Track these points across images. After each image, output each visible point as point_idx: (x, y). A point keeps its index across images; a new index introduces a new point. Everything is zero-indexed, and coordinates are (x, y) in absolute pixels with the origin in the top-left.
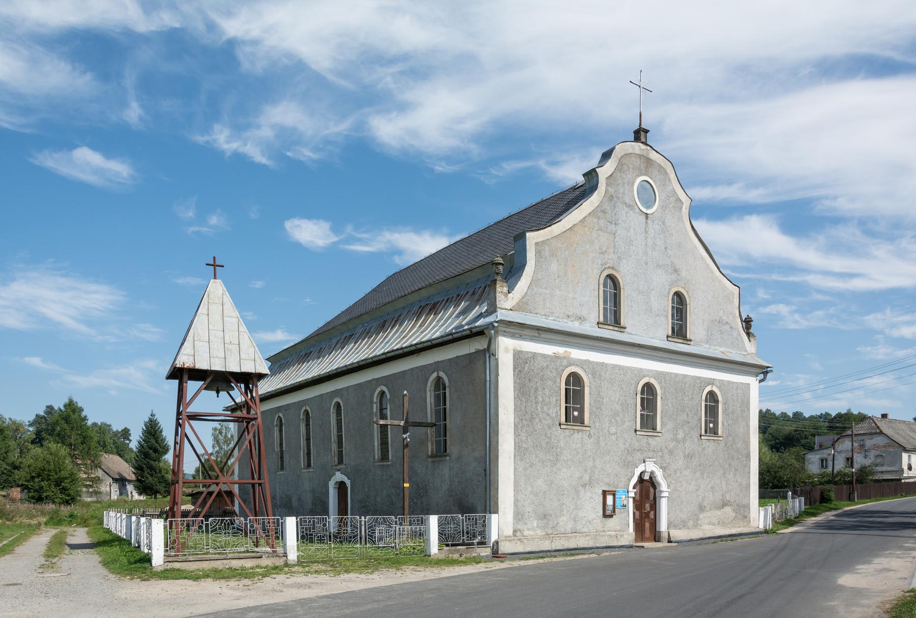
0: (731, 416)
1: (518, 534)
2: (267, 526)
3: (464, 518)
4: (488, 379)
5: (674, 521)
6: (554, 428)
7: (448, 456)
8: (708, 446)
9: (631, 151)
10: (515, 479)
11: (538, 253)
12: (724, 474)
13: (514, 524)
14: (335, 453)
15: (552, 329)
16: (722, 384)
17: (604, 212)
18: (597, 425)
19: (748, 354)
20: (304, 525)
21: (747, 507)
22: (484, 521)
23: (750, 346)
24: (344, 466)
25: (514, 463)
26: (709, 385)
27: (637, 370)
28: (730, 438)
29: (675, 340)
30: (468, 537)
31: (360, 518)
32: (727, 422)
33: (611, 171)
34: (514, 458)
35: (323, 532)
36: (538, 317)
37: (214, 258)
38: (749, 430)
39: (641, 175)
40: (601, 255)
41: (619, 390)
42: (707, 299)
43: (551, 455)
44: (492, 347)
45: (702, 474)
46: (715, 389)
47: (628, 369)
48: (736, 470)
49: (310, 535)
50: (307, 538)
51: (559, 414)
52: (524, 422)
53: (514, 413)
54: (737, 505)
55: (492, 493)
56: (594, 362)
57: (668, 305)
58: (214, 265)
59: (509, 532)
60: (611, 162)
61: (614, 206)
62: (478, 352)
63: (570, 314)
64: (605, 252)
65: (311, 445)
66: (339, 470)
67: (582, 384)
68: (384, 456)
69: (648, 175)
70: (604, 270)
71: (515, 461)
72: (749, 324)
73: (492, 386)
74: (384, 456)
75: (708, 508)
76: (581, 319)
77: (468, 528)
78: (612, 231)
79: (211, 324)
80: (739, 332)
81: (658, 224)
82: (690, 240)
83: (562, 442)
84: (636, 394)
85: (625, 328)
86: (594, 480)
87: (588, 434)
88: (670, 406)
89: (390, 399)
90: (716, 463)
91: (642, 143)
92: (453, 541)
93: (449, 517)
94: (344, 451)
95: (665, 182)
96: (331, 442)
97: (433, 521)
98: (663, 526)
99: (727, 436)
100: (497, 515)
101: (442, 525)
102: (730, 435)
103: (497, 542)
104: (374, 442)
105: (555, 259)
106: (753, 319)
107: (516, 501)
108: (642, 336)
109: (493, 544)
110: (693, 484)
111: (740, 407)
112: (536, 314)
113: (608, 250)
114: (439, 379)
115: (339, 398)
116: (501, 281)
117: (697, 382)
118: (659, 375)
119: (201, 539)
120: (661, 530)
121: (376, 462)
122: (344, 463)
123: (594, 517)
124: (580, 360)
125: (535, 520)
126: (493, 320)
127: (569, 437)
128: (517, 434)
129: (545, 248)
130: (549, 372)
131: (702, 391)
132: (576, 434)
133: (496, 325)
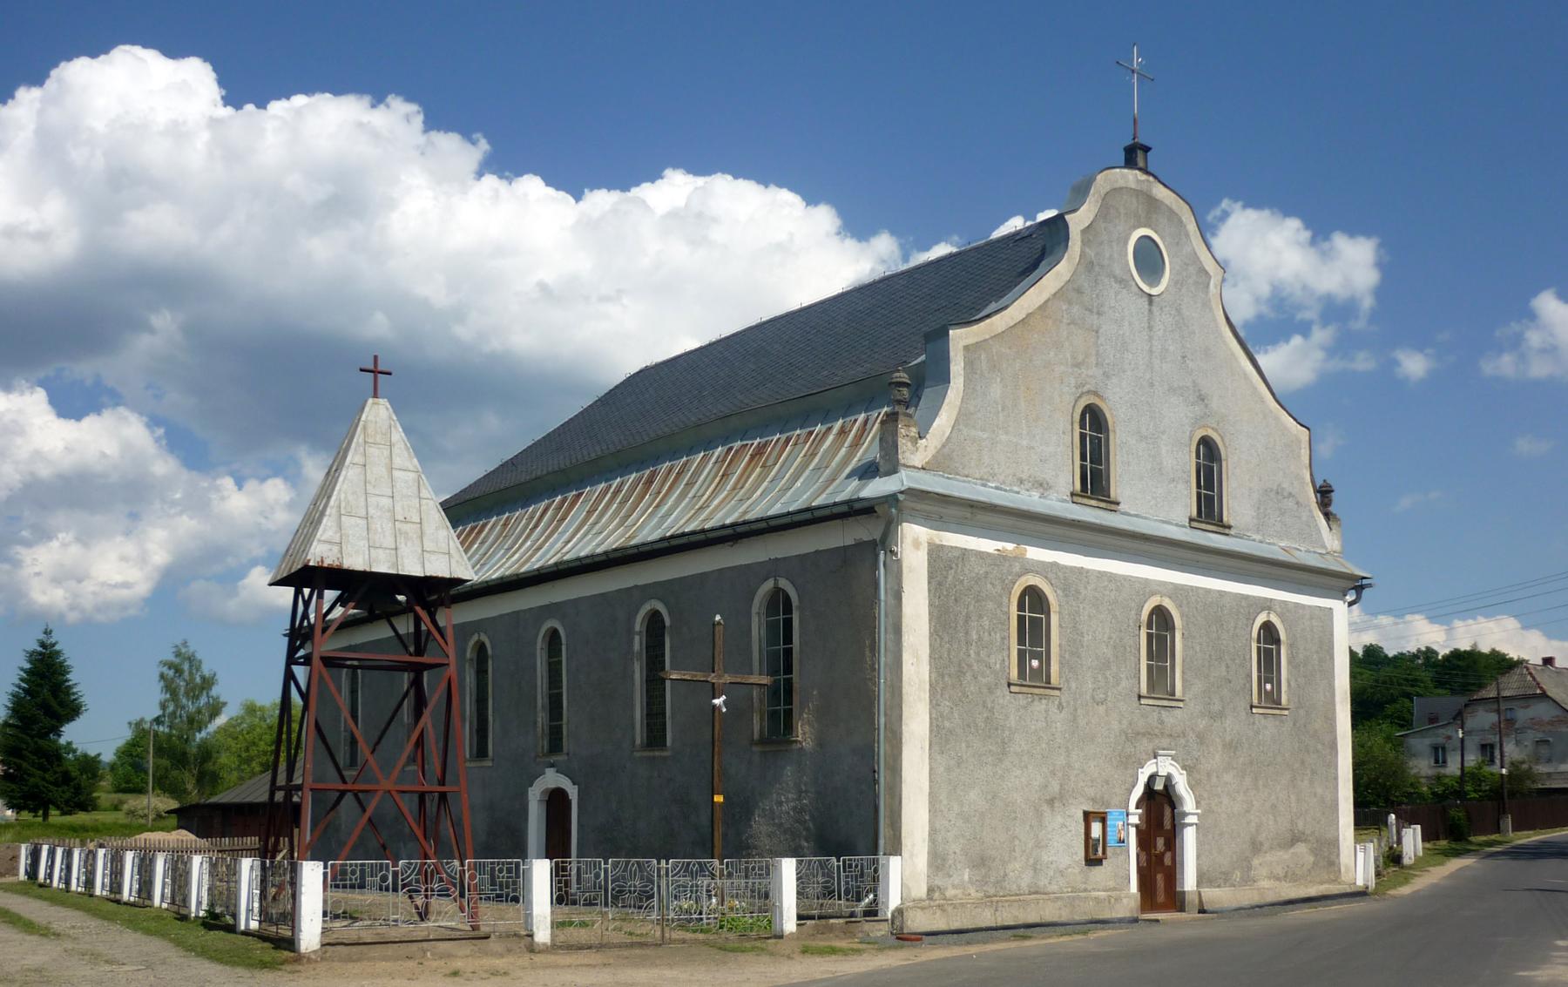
2: (499, 878)
3: (841, 863)
6: (999, 692)
9: (1121, 183)
11: (970, 365)
13: (928, 876)
14: (543, 729)
16: (1285, 609)
18: (1073, 685)
21: (1334, 843)
25: (930, 759)
26: (1262, 610)
28: (1302, 712)
29: (1203, 526)
31: (659, 863)
32: (1296, 681)
34: (930, 749)
36: (969, 482)
40: (1076, 369)
45: (1256, 779)
46: (1274, 619)
47: (1125, 580)
48: (1314, 772)
51: (1007, 664)
52: (946, 679)
53: (930, 662)
56: (1066, 567)
57: (1188, 461)
58: (375, 372)
59: (920, 891)
62: (860, 545)
63: (1024, 476)
66: (552, 766)
70: (1080, 397)
74: (655, 735)
75: (1266, 846)
76: (1043, 486)
77: (847, 883)
78: (1092, 325)
80: (1311, 511)
83: (1012, 717)
84: (1140, 627)
85: (1118, 504)
87: (1057, 703)
88: (1198, 648)
89: (671, 626)
91: (1140, 169)
96: (536, 707)
98: (1189, 881)
103: (899, 912)
107: (933, 832)
108: (1146, 518)
112: (967, 476)
113: (1087, 360)
117: (1243, 604)
118: (1177, 591)
122: (565, 749)
125: (965, 868)
128: (934, 702)
129: (980, 355)
130: (989, 586)
132: (1036, 703)
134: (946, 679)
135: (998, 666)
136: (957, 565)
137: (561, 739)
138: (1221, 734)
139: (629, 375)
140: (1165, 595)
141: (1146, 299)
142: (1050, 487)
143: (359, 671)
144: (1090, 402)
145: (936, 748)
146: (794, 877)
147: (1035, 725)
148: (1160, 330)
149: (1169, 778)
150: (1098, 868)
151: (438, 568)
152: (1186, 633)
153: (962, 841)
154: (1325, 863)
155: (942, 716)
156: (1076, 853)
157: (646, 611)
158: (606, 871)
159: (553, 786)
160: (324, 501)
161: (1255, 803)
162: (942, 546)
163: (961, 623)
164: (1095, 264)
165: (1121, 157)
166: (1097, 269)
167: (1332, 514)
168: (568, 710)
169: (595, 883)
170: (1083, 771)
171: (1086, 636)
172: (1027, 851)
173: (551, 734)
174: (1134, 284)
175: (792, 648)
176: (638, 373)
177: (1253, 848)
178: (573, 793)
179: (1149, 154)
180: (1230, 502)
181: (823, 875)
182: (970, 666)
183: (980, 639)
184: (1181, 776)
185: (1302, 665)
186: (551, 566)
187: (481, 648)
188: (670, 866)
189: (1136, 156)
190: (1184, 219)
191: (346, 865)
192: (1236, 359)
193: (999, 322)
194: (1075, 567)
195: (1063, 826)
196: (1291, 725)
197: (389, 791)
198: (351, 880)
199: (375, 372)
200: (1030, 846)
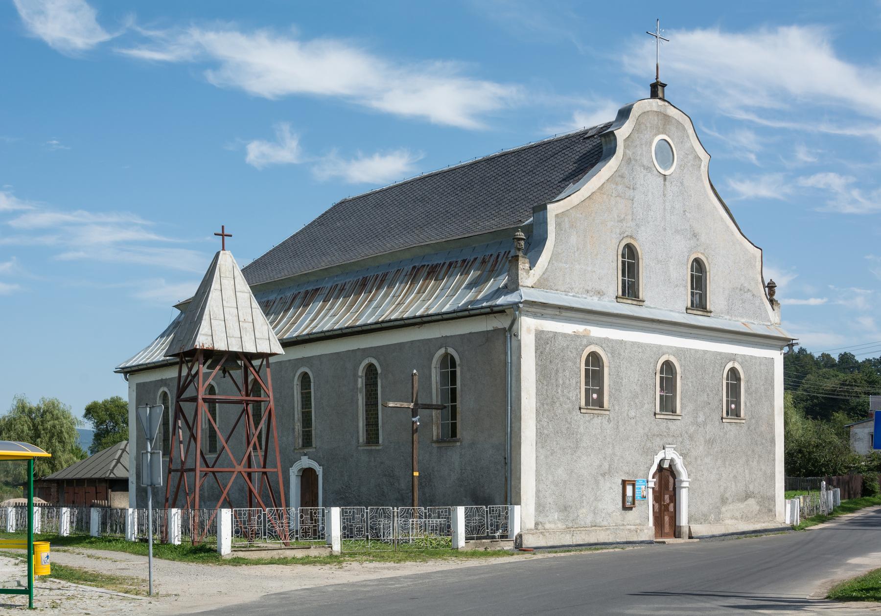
4: (509, 361)
5: (695, 514)
7: (458, 441)
9: (648, 109)
11: (558, 225)
12: (747, 461)
13: (535, 517)
14: (299, 434)
16: (744, 360)
17: (622, 177)
18: (617, 408)
21: (772, 499)
22: (507, 513)
25: (536, 451)
28: (753, 421)
29: (695, 312)
30: (492, 530)
32: (750, 402)
33: (629, 132)
40: (619, 224)
41: (638, 370)
45: (724, 461)
46: (737, 366)
48: (760, 456)
50: (242, 532)
51: (579, 397)
52: (545, 406)
53: (536, 397)
54: (762, 497)
56: (613, 340)
58: (223, 235)
59: (531, 525)
60: (629, 122)
62: (496, 330)
63: (589, 288)
66: (305, 455)
69: (665, 134)
71: (536, 449)
74: (372, 436)
75: (730, 500)
77: (491, 520)
80: (761, 300)
82: (709, 200)
89: (381, 373)
90: (739, 449)
91: (660, 99)
92: (478, 534)
97: (335, 513)
98: (684, 520)
104: (358, 422)
107: (538, 491)
110: (714, 472)
111: (764, 385)
112: (557, 290)
113: (626, 217)
116: (523, 257)
118: (680, 352)
120: (681, 525)
121: (360, 446)
122: (314, 446)
126: (517, 300)
127: (589, 421)
130: (569, 353)
131: (723, 368)
132: (595, 419)
134: (545, 406)
135: (574, 398)
136: (551, 341)
140: (671, 354)
141: (662, 179)
142: (604, 294)
143: (217, 404)
145: (540, 445)
149: (672, 460)
150: (630, 511)
152: (683, 376)
158: (367, 512)
164: (632, 159)
166: (633, 162)
167: (775, 301)
169: (361, 519)
170: (622, 457)
171: (624, 379)
175: (456, 388)
177: (722, 501)
178: (319, 470)
182: (558, 398)
183: (564, 383)
184: (679, 460)
185: (754, 393)
189: (658, 91)
190: (686, 126)
191: (241, 510)
193: (576, 199)
195: (611, 488)
197: (240, 472)
198: (244, 518)
199: (223, 235)
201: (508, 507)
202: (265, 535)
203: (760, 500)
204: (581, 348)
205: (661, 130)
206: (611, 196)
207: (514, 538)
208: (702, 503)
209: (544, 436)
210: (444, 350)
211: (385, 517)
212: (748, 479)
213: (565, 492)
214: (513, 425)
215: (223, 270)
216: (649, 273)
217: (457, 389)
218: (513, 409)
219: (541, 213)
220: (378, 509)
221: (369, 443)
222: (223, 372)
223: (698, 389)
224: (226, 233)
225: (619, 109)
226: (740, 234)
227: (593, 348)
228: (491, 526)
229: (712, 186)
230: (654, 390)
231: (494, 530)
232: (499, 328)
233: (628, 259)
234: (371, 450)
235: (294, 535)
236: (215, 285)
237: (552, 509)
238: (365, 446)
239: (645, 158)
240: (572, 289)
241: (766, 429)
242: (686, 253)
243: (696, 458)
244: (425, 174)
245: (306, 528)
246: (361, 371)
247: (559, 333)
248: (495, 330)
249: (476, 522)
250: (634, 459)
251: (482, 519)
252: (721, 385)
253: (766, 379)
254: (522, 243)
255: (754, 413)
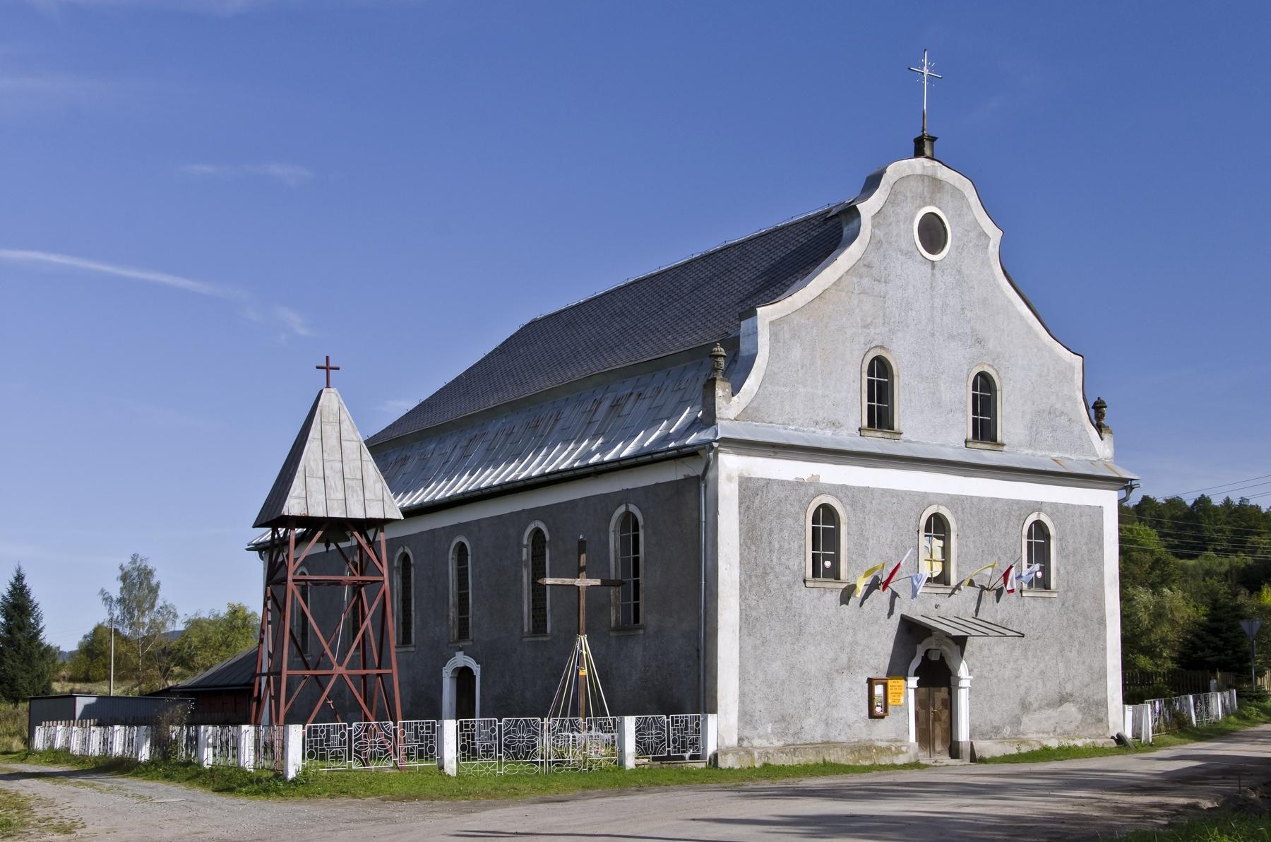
0: (1072, 558)
1: (745, 744)
2: (420, 733)
3: (670, 720)
4: (703, 520)
5: (980, 725)
6: (796, 588)
7: (641, 628)
8: (1034, 608)
9: (909, 172)
10: (740, 663)
11: (774, 336)
12: (1062, 650)
13: (739, 729)
14: (454, 621)
15: (793, 445)
16: (1055, 509)
17: (868, 267)
19: (1099, 460)
20: (465, 731)
21: (1103, 704)
22: (698, 725)
23: (1102, 447)
24: (471, 643)
25: (740, 640)
27: (919, 496)
29: (979, 445)
30: (675, 747)
31: (542, 720)
32: (1065, 568)
33: (879, 205)
34: (740, 632)
35: (491, 740)
37: (327, 358)
38: (1102, 579)
39: (925, 205)
40: (865, 330)
41: (891, 526)
42: (1030, 380)
43: (792, 626)
44: (710, 475)
45: (1026, 650)
46: (1044, 518)
48: (1082, 644)
49: (321, 750)
50: (317, 755)
51: (803, 565)
52: (753, 578)
53: (740, 566)
54: (1085, 701)
55: (708, 684)
56: (854, 488)
58: (328, 368)
59: (732, 741)
60: (880, 192)
61: (884, 256)
62: (688, 479)
64: (871, 324)
65: (413, 608)
66: (460, 650)
67: (836, 521)
68: (539, 624)
69: (934, 204)
70: (869, 351)
71: (740, 637)
72: (1101, 412)
73: (709, 529)
74: (539, 624)
75: (1035, 705)
76: (834, 424)
77: (674, 734)
78: (880, 292)
79: (326, 452)
81: (951, 275)
82: (1002, 292)
84: (918, 531)
86: (855, 663)
88: (972, 546)
89: (550, 541)
90: (1048, 634)
92: (654, 754)
93: (650, 719)
94: (470, 619)
95: (962, 210)
97: (630, 723)
98: (963, 735)
99: (1065, 591)
100: (716, 715)
101: (640, 730)
102: (1069, 589)
103: (716, 756)
104: (522, 606)
105: (797, 342)
106: (1107, 404)
107: (742, 695)
109: (710, 758)
110: (1010, 667)
111: (1086, 544)
112: (771, 423)
113: (874, 321)
114: (628, 515)
115: (464, 538)
116: (722, 380)
118: (955, 501)
119: (343, 750)
121: (525, 637)
122: (471, 637)
123: (855, 719)
124: (834, 486)
125: (768, 723)
126: (711, 438)
127: (819, 599)
128: (743, 596)
129: (783, 327)
130: (789, 506)
131: (1022, 522)
132: (828, 595)
133: (715, 445)
135: (796, 567)
137: (468, 629)
138: (993, 614)
139: (522, 326)
140: (942, 504)
142: (841, 426)
144: (878, 354)
146: (634, 730)
147: (827, 612)
148: (941, 289)
150: (882, 720)
151: (375, 512)
152: (960, 534)
153: (766, 702)
154: (1094, 720)
155: (750, 607)
156: (862, 711)
157: (532, 529)
158: (500, 726)
159: (462, 665)
160: (293, 467)
161: (1024, 670)
162: (750, 478)
163: (765, 535)
164: (884, 241)
165: (912, 146)
166: (885, 246)
167: (1104, 426)
168: (473, 606)
170: (868, 647)
171: (871, 540)
172: (820, 709)
173: (460, 625)
174: (919, 254)
176: (529, 324)
177: (1023, 707)
178: (477, 669)
179: (935, 143)
180: (1004, 424)
181: (656, 728)
183: (781, 547)
185: (1071, 555)
186: (459, 494)
187: (405, 557)
188: (551, 723)
189: (924, 147)
191: (317, 726)
192: (1013, 305)
194: (862, 487)
195: (851, 689)
196: (1060, 606)
197: (342, 675)
198: (320, 736)
199: (327, 368)
200: (822, 705)
201: (699, 716)
202: (350, 759)
203: (1083, 705)
204: (806, 499)
205: (927, 200)
206: (853, 293)
207: (708, 759)
208: (991, 709)
209: (751, 619)
210: (625, 507)
211: (529, 731)
212: (1063, 676)
213: (783, 695)
214: (708, 606)
215: (325, 413)
216: (908, 395)
217: (640, 559)
218: (708, 583)
219: (750, 320)
220: (517, 721)
221: (536, 633)
222: (326, 545)
223: (983, 551)
224: (331, 365)
225: (868, 175)
226: (1050, 337)
227: (824, 499)
228: (674, 742)
229: (1005, 272)
230: (916, 553)
231: (679, 748)
232: (692, 475)
233: (877, 377)
234: (538, 641)
235: (391, 757)
236: (314, 433)
237: (764, 718)
238: (531, 637)
239: (902, 240)
240: (793, 420)
241: (1091, 605)
242: (965, 366)
243: (981, 648)
244: (631, 280)
245: (408, 748)
246: (526, 540)
247: (774, 480)
248: (687, 478)
249: (652, 738)
250: (885, 648)
251: (660, 734)
252: (1018, 545)
253: (1091, 535)
254: (722, 361)
255: (1072, 583)
